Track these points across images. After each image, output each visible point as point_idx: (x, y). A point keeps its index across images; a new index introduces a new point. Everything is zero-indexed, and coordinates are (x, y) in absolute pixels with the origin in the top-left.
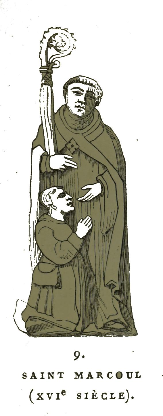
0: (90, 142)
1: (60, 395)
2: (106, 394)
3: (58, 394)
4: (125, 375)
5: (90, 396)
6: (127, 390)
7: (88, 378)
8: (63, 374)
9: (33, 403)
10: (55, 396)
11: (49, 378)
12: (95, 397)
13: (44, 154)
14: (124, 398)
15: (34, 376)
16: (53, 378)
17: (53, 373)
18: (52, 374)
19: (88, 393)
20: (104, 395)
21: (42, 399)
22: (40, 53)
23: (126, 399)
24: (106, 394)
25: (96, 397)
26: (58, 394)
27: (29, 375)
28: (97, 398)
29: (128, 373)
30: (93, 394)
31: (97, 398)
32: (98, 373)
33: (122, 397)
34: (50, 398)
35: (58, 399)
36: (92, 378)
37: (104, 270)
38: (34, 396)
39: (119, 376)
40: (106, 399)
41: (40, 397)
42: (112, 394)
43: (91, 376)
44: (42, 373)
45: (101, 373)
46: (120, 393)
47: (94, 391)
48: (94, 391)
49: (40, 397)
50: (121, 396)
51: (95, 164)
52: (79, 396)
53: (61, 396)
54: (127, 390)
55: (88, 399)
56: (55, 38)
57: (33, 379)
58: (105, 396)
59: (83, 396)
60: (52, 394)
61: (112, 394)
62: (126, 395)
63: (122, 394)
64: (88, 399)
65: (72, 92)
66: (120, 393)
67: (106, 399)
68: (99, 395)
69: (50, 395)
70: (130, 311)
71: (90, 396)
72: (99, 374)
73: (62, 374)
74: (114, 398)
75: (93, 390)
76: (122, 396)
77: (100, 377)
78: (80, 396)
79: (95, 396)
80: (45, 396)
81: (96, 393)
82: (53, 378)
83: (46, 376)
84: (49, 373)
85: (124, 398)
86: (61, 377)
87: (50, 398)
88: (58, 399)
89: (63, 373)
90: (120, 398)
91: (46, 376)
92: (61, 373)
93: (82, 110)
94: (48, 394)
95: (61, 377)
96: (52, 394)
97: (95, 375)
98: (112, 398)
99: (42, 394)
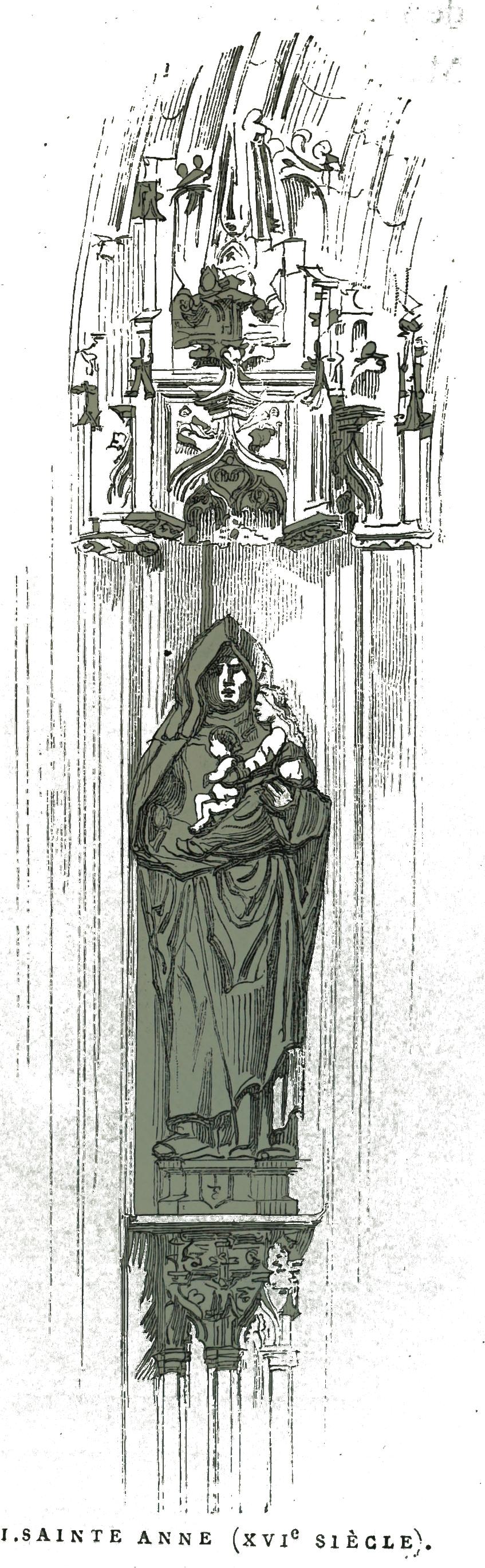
1: (289, 1539)
3: (285, 1536)
5: (342, 1542)
10: (277, 1541)
12: (406, 1545)
14: (411, 1547)
20: (370, 1540)
21: (253, 1545)
23: (414, 1550)
24: (373, 1538)
26: (285, 1536)
27: (35, 1534)
28: (209, 1543)
30: (349, 1537)
31: (120, 1541)
34: (268, 1544)
38: (241, 1540)
41: (249, 1540)
42: (387, 1538)
43: (45, 1535)
46: (403, 1537)
47: (352, 1531)
48: (352, 1531)
49: (250, 1539)
51: (392, 794)
52: (320, 1542)
57: (43, 1543)
58: (371, 1543)
59: (329, 1541)
60: (272, 1535)
61: (387, 1538)
62: (414, 1541)
65: (241, 48)
66: (403, 1537)
67: (374, 1547)
68: (361, 1541)
69: (268, 1538)
71: (342, 1542)
74: (392, 1547)
78: (29, 1536)
83: (67, 1536)
85: (411, 1547)
86: (96, 1540)
87: (268, 1544)
88: (284, 1545)
90: (202, 1543)
92: (97, 1532)
94: (265, 1536)
95: (96, 1540)
96: (272, 1535)
97: (154, 1537)
98: (386, 1546)
99: (253, 1535)
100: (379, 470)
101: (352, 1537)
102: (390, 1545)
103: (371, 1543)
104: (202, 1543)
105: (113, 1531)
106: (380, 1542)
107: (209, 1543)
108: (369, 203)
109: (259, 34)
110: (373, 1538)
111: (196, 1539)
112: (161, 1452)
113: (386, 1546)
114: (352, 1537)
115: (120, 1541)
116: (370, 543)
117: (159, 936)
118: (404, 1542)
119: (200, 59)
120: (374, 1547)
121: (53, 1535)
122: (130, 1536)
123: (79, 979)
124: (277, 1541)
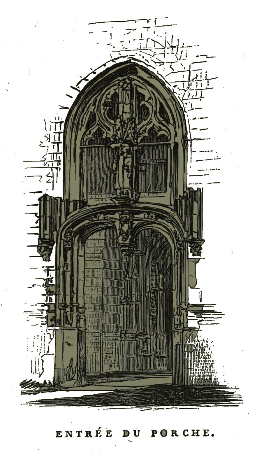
0: (172, 63)
2: (187, 430)
4: (132, 433)
8: (82, 432)
11: (71, 432)
12: (206, 434)
16: (71, 436)
17: (71, 432)
18: (70, 433)
19: (152, 436)
20: (186, 432)
22: (45, 338)
24: (187, 430)
25: (110, 435)
29: (135, 431)
31: (101, 436)
32: (87, 432)
33: (99, 435)
36: (91, 436)
39: (164, 433)
40: (188, 435)
45: (90, 432)
46: (205, 430)
50: (206, 433)
53: (158, 435)
55: (80, 436)
56: (53, 278)
58: (186, 433)
63: (206, 431)
64: (80, 436)
66: (205, 430)
67: (188, 435)
73: (80, 432)
74: (76, 431)
76: (207, 432)
77: (174, 435)
79: (99, 433)
81: (101, 431)
82: (71, 436)
84: (67, 432)
86: (79, 436)
89: (81, 432)
92: (79, 432)
93: (115, 96)
95: (79, 436)
102: (77, 432)
103: (186, 433)
104: (107, 436)
105: (107, 431)
107: (111, 436)
108: (160, 65)
109: (141, 33)
111: (201, 433)
112: (169, 408)
115: (111, 436)
118: (205, 433)
119: (204, 251)
121: (180, 433)
123: (229, 387)
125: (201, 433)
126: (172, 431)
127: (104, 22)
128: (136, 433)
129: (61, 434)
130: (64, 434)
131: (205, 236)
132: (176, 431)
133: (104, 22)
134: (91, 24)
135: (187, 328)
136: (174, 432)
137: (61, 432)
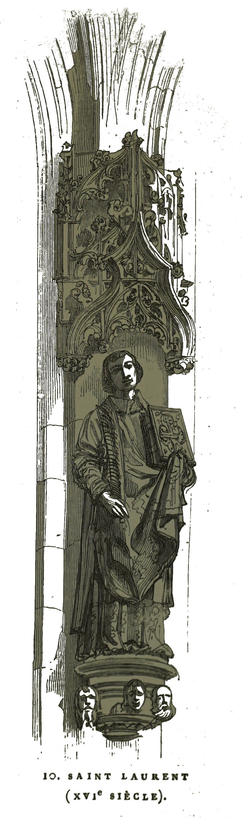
1: (97, 795)
2: (138, 794)
5: (123, 796)
6: (160, 791)
7: (132, 779)
9: (69, 802)
10: (91, 796)
11: (100, 774)
13: (176, 331)
15: (80, 776)
16: (100, 779)
17: (100, 774)
23: (158, 800)
24: (51, 779)
27: (75, 776)
32: (153, 775)
35: (94, 799)
37: (80, 437)
38: (71, 797)
42: (144, 795)
44: (89, 774)
45: (156, 775)
49: (77, 797)
52: (112, 796)
54: (160, 791)
58: (137, 796)
59: (116, 796)
61: (144, 795)
62: (158, 796)
67: (138, 799)
68: (131, 796)
69: (87, 795)
70: (170, 650)
72: (165, 776)
75: (127, 792)
80: (81, 796)
82: (100, 779)
83: (93, 776)
86: (108, 778)
91: (93, 776)
95: (108, 778)
98: (144, 799)
100: (136, 355)
101: (127, 795)
102: (125, 777)
106: (141, 797)
110: (138, 794)
113: (144, 799)
114: (127, 795)
116: (162, 569)
117: (163, 347)
120: (138, 799)
121: (85, 776)
122: (191, 497)
124: (91, 796)
125: (170, 776)
126: (153, 775)
127: (161, 730)
128: (134, 777)
129: (168, 776)
130: (170, 776)
131: (196, 459)
132: (156, 775)
133: (161, 730)
134: (161, 736)
135: (167, 409)
136: (155, 776)
137: (167, 774)
